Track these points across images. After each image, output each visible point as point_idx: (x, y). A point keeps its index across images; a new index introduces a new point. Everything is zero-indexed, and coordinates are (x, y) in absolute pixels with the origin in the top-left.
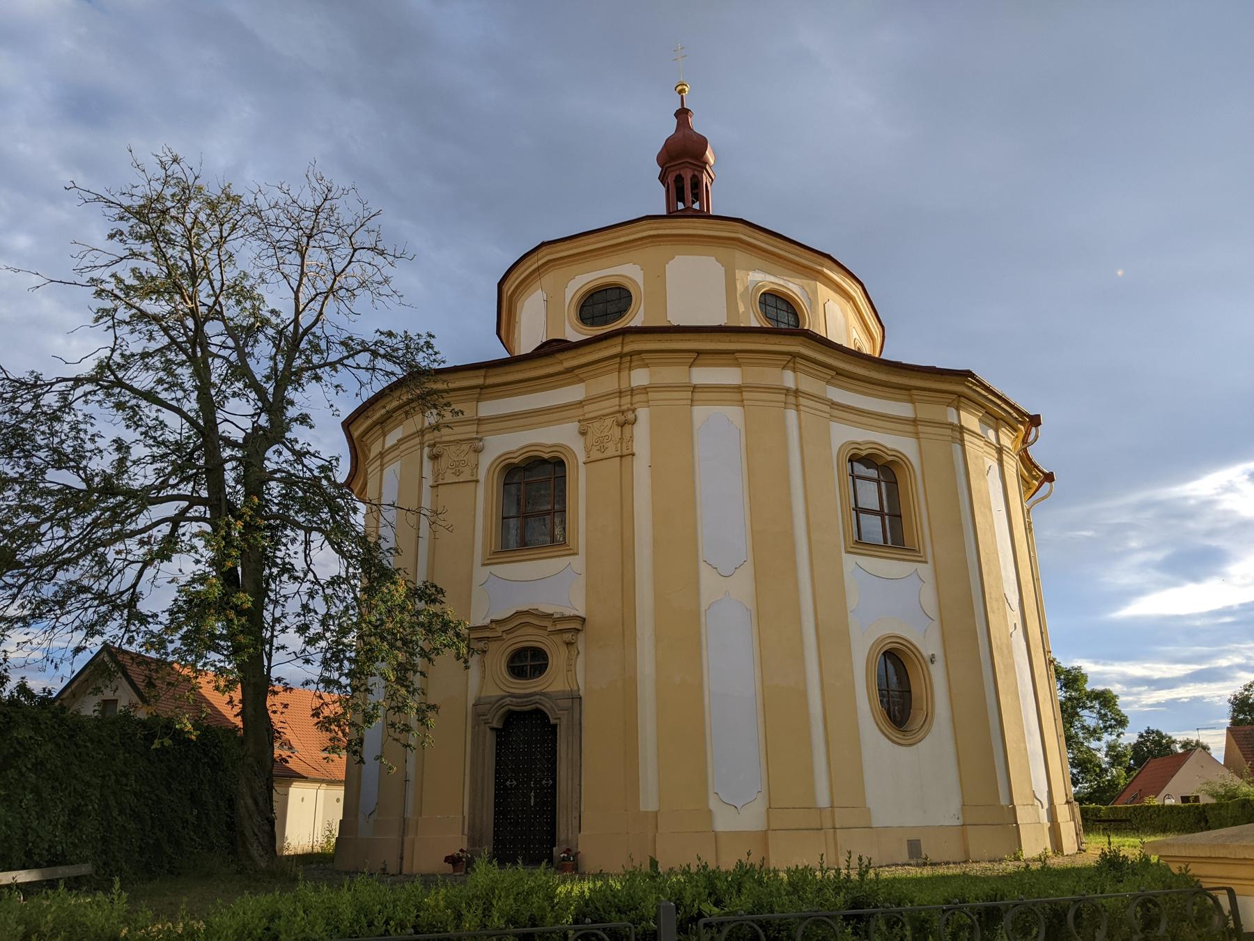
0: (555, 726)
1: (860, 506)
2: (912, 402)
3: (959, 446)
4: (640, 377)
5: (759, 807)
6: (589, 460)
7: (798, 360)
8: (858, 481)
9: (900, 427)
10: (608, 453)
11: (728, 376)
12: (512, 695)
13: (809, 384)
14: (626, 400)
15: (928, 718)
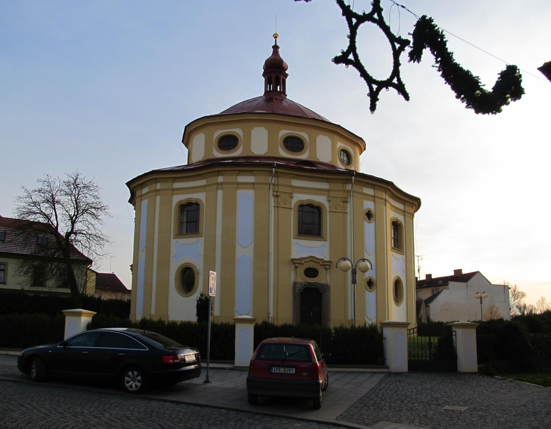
3: (385, 206)
7: (388, 191)
9: (399, 212)
11: (250, 179)
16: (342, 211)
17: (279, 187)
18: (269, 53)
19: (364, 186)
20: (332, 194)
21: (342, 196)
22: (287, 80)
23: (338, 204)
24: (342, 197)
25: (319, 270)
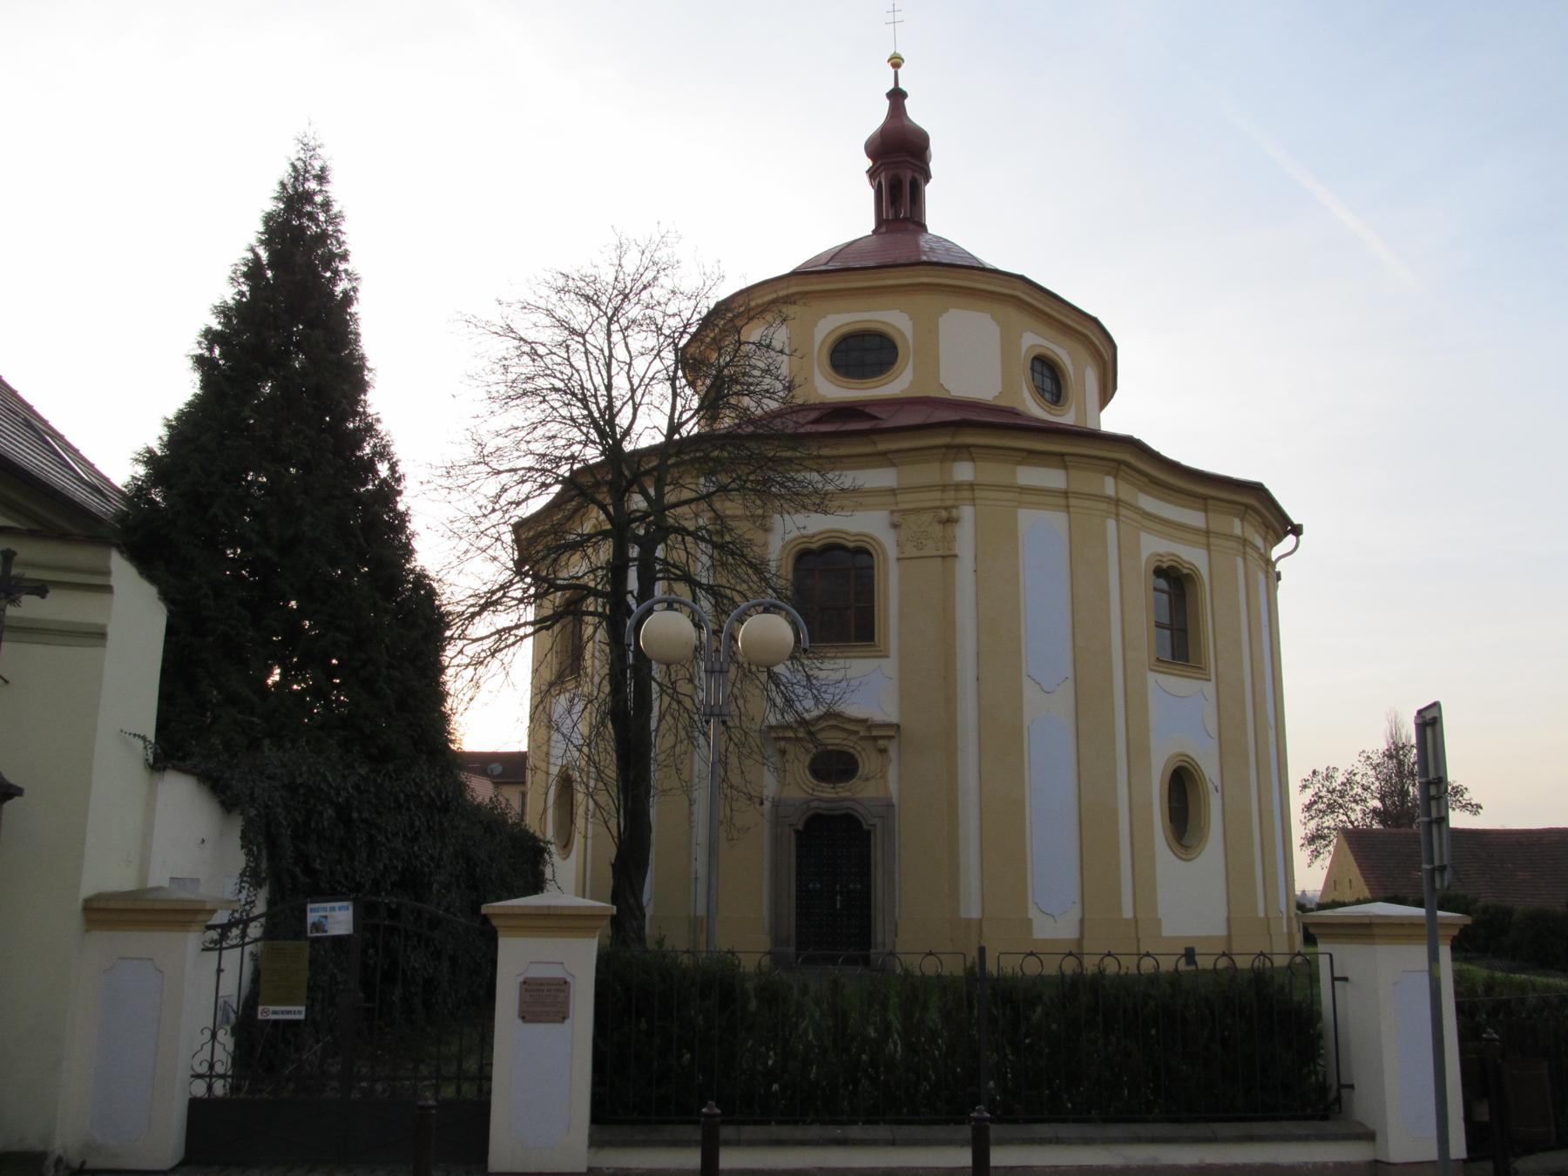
0: (869, 832)
2: (1206, 511)
4: (964, 471)
5: (1075, 914)
6: (903, 556)
7: (1123, 468)
11: (1053, 478)
12: (819, 799)
13: (1127, 492)
15: (1202, 834)
16: (940, 553)
17: (976, 492)
18: (876, 116)
19: (1019, 463)
20: (907, 501)
21: (938, 503)
23: (924, 532)
24: (938, 508)
25: (860, 760)
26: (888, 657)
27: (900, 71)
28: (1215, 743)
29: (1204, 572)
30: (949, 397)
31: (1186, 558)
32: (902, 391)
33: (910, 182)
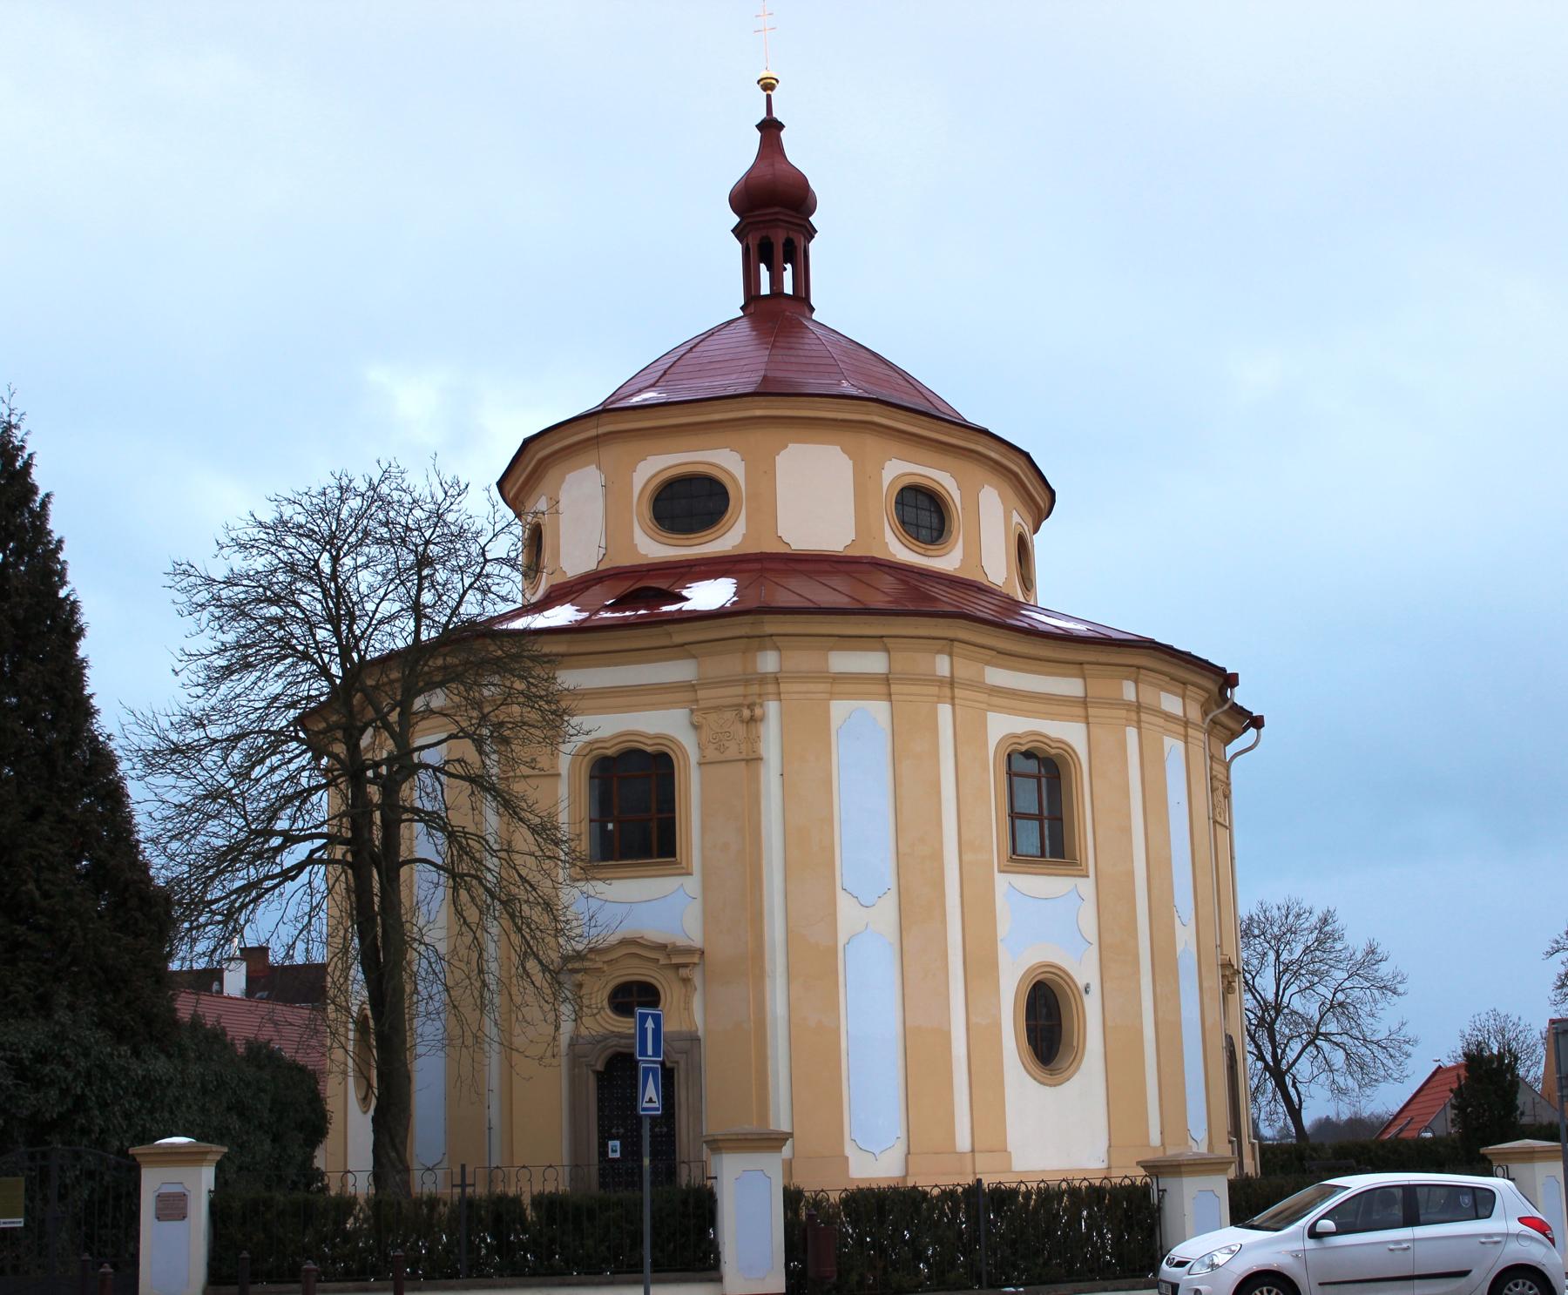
1: (1016, 811)
3: (444, 736)
4: (769, 662)
5: (899, 1150)
8: (1015, 779)
9: (1064, 709)
10: (729, 755)
11: (873, 662)
13: (965, 670)
14: (755, 689)
15: (1077, 1054)
18: (743, 154)
22: (814, 247)
26: (690, 874)
27: (774, 94)
28: (1095, 949)
29: (1081, 748)
30: (789, 551)
31: (1053, 734)
32: (733, 547)
33: (784, 245)
